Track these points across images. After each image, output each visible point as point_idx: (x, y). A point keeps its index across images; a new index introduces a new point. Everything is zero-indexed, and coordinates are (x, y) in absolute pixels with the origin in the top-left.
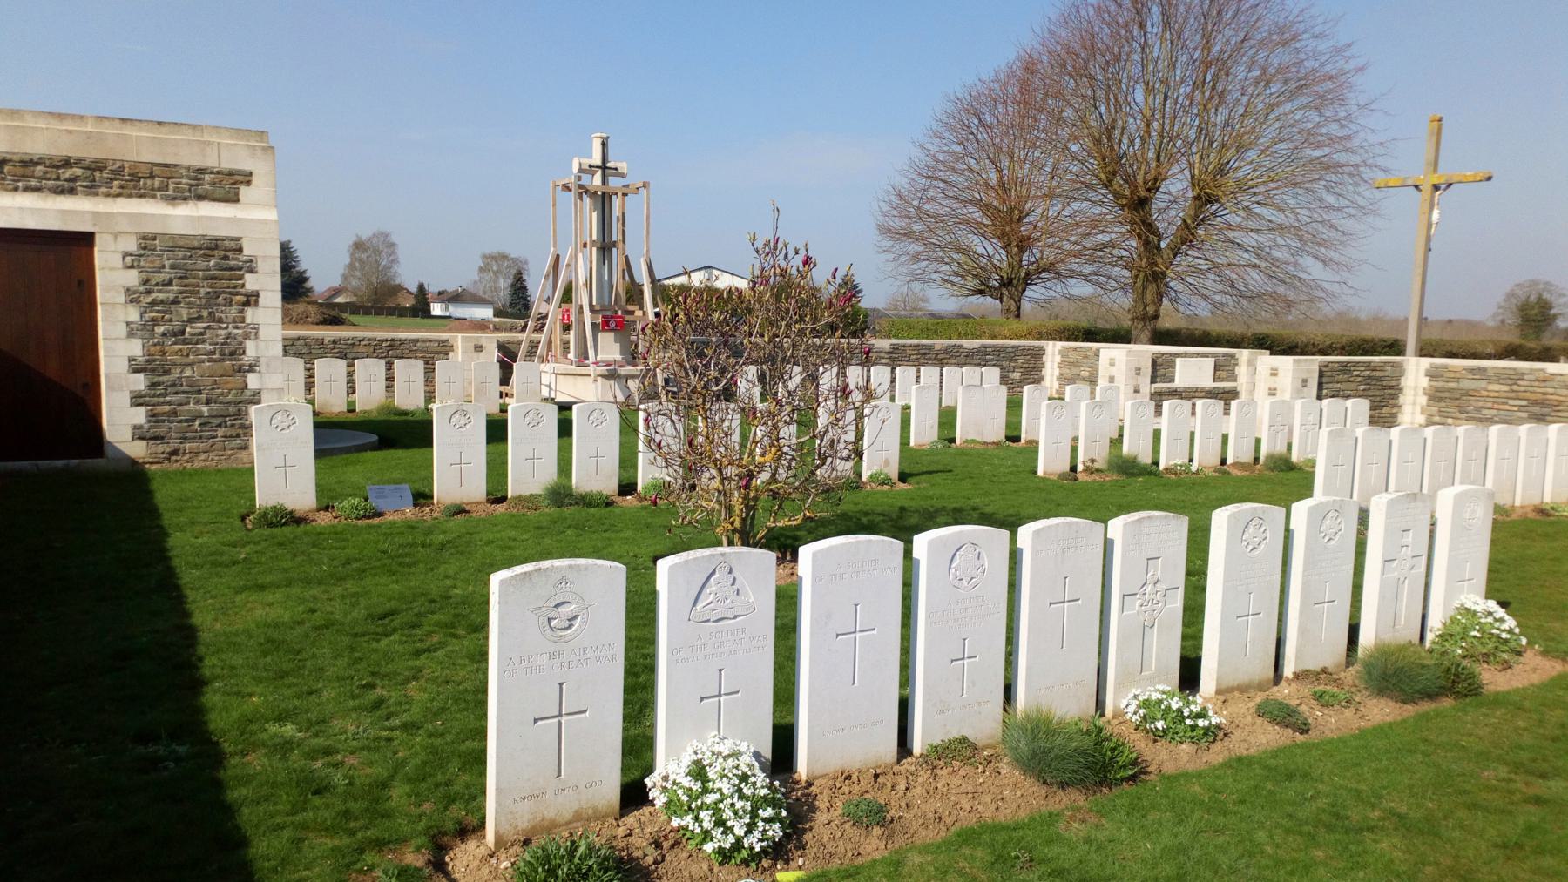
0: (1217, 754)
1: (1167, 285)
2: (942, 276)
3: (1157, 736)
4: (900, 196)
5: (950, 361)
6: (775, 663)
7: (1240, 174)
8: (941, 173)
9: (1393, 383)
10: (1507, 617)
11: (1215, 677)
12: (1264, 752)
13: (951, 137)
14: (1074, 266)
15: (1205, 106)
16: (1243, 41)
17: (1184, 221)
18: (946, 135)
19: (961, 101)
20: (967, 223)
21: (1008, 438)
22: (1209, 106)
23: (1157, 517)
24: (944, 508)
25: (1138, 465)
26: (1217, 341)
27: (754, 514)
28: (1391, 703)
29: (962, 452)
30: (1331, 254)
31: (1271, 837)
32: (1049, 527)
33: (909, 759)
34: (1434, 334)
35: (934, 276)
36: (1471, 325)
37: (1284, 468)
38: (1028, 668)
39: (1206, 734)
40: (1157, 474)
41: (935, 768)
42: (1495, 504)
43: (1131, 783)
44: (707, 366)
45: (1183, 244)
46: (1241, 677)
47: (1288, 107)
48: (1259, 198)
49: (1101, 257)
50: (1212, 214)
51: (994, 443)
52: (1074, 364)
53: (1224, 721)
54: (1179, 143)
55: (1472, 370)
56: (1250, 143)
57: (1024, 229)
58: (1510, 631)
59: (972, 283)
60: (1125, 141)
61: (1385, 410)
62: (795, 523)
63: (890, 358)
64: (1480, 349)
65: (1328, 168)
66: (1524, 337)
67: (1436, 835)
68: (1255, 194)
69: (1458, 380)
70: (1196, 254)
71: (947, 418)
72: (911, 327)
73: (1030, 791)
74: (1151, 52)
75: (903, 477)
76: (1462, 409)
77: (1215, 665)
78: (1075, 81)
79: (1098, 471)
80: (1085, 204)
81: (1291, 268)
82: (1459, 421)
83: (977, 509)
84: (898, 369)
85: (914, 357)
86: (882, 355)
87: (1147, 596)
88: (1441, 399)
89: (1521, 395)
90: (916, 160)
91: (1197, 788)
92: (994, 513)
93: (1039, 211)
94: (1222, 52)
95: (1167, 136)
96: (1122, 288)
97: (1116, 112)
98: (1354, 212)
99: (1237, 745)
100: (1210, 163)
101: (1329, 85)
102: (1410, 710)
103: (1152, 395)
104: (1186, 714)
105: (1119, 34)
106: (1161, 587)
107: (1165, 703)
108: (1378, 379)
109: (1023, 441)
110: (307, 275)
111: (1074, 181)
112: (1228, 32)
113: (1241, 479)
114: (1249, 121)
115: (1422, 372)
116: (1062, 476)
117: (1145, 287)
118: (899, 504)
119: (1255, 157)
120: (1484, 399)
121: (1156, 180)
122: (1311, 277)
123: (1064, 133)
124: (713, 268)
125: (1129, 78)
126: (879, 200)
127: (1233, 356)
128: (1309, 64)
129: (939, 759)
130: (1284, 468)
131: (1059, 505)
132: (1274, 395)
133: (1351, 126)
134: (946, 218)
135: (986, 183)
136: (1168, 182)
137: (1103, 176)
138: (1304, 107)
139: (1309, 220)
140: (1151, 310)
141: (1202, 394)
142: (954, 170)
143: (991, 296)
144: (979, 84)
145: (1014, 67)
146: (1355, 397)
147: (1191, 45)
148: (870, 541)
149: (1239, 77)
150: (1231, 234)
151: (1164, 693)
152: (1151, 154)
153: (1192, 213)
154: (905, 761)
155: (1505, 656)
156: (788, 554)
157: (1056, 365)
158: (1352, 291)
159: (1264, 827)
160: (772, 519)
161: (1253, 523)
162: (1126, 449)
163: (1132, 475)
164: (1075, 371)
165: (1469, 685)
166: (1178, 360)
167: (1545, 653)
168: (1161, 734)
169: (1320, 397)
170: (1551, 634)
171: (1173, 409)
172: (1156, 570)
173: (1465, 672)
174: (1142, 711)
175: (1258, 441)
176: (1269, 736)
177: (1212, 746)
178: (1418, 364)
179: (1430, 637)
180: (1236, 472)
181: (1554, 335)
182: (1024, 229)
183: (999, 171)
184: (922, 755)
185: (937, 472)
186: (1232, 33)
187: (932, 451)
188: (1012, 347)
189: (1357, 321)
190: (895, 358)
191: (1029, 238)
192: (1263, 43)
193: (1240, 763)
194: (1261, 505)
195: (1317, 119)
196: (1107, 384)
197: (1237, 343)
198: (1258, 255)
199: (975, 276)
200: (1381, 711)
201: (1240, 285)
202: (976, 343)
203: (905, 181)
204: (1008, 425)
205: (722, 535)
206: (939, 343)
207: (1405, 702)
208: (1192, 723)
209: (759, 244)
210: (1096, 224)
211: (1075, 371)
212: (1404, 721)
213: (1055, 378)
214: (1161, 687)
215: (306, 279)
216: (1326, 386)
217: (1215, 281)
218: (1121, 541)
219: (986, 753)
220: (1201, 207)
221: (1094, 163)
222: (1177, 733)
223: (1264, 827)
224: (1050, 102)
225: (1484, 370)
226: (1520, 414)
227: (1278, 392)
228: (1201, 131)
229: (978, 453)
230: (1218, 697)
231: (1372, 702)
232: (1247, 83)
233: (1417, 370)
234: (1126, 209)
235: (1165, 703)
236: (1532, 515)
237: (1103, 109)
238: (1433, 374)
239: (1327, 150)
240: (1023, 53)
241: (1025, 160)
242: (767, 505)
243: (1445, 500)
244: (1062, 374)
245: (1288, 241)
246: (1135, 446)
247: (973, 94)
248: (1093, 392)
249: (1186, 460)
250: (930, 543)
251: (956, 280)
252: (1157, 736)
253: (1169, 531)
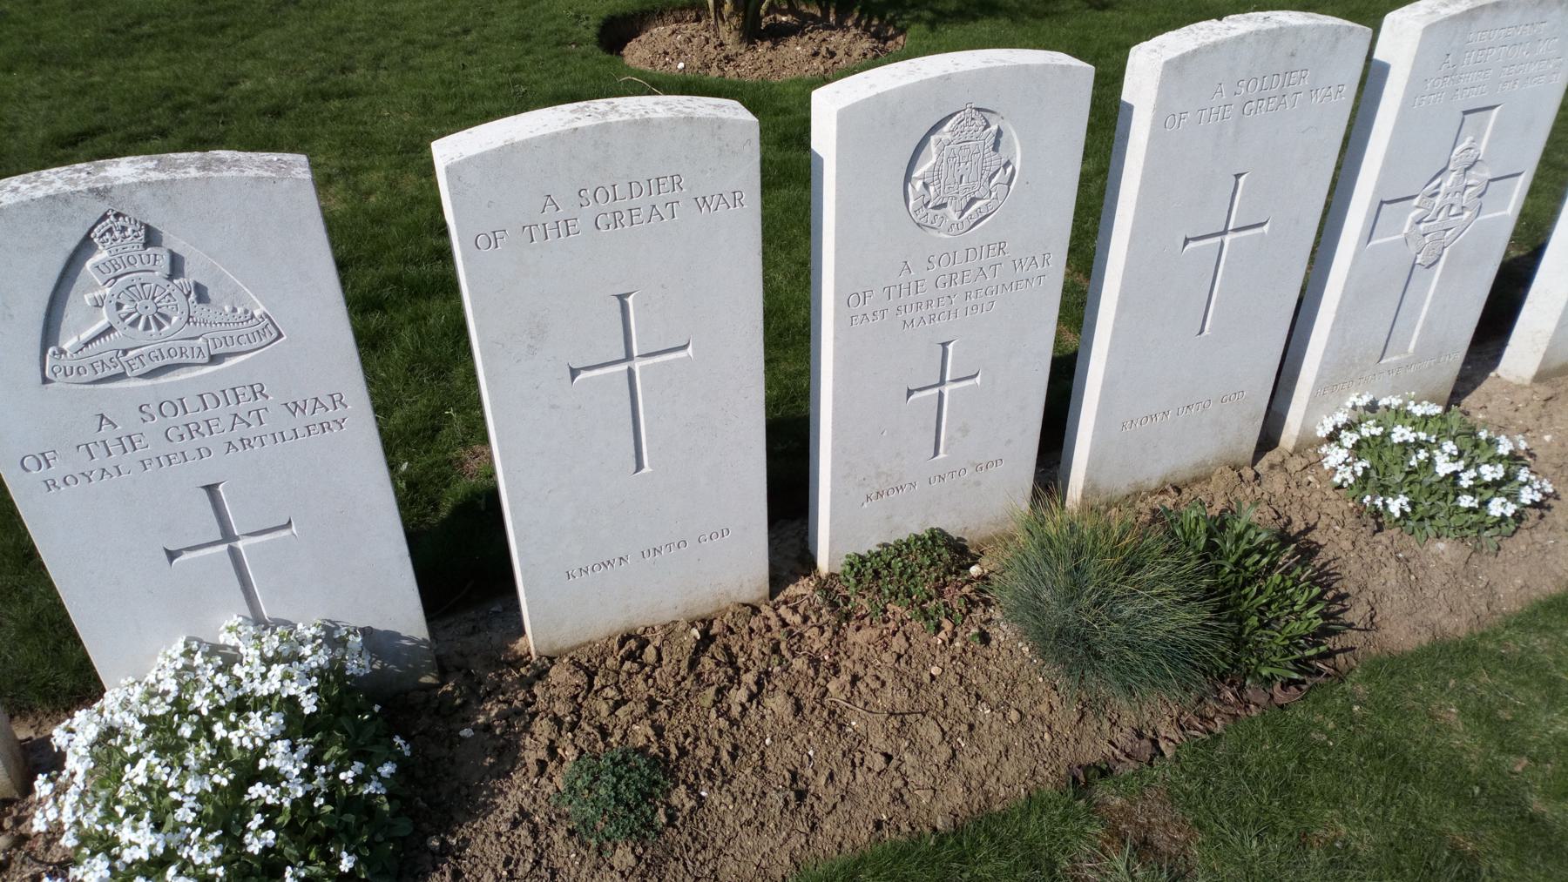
6: (765, 219)
11: (1543, 348)
87: (1438, 200)
148: (646, 123)
156: (832, 11)
177: (1507, 543)
218: (1407, 71)
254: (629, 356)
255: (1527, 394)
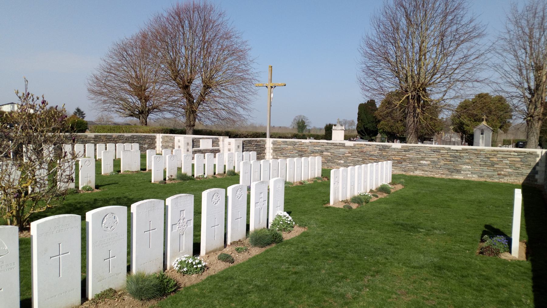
0: (205, 276)
1: (196, 115)
2: (116, 109)
3: (184, 273)
4: (97, 78)
5: (120, 141)
7: (217, 79)
8: (113, 71)
9: (263, 146)
10: (289, 217)
12: (219, 272)
13: (116, 58)
14: (165, 107)
15: (205, 56)
16: (215, 36)
17: (201, 94)
18: (114, 57)
19: (119, 45)
20: (124, 90)
21: (141, 169)
22: (206, 56)
23: (183, 196)
24: (113, 198)
25: (187, 176)
26: (214, 134)
27: (23, 208)
28: (258, 248)
29: (123, 176)
30: (245, 106)
31: (219, 303)
32: (143, 203)
33: (87, 302)
34: (275, 131)
35: (113, 109)
36: (285, 128)
37: (233, 174)
38: (137, 257)
39: (201, 270)
40: (193, 179)
41: (98, 303)
42: (286, 183)
43: (174, 293)
45: (201, 101)
46: (214, 247)
47: (230, 59)
48: (223, 87)
49: (174, 104)
50: (210, 92)
51: (136, 171)
52: (167, 142)
53: (207, 264)
54: (197, 68)
55: (283, 142)
56: (219, 70)
57: (147, 94)
58: (290, 221)
59: (128, 112)
60: (180, 65)
61: (262, 154)
62: (43, 210)
63: (94, 140)
64: (287, 135)
65: (243, 79)
66: (299, 131)
67: (268, 290)
68: (222, 86)
69: (280, 145)
70: (205, 105)
71: (117, 163)
72: (104, 128)
73: (136, 304)
74: (186, 36)
75: (97, 187)
76: (282, 154)
77: (205, 244)
78: (161, 43)
79: (173, 179)
80: (168, 86)
81: (234, 110)
82: (281, 157)
83: (126, 197)
84: (97, 145)
85: (105, 140)
86: (91, 139)
88: (276, 151)
89: (296, 149)
90: (103, 66)
91: (196, 290)
92: (133, 198)
93: (152, 87)
94: (209, 39)
95: (193, 65)
96: (182, 115)
97: (176, 55)
98: (251, 93)
99: (211, 272)
100: (208, 75)
101: (241, 53)
102: (264, 249)
103: (193, 152)
104: (194, 264)
105: (175, 28)
106: (186, 220)
107: (187, 261)
108: (259, 145)
109: (147, 170)
111: (163, 78)
112: (210, 33)
113: (219, 179)
114: (219, 63)
115: (271, 143)
116: (161, 182)
117: (190, 116)
118: (94, 198)
119: (221, 74)
120: (287, 150)
121: (191, 79)
122: (240, 113)
123: (159, 61)
124: (15, 104)
125: (180, 44)
126: (88, 79)
127: (218, 139)
128: (235, 46)
129: (100, 299)
130: (233, 174)
131: (158, 193)
132: (230, 151)
133: (248, 67)
134: (116, 88)
135: (132, 77)
136: (195, 80)
137: (173, 77)
138: (234, 59)
139: (238, 95)
140: (192, 123)
141: (209, 151)
142: (118, 70)
143: (136, 117)
144: (125, 40)
145: (139, 36)
146: (253, 151)
147: (199, 35)
148: (65, 217)
149: (215, 48)
150: (215, 99)
151: (187, 258)
152: (189, 71)
153: (203, 91)
154: (85, 303)
155: (289, 228)
157: (160, 142)
158: (251, 118)
159: (217, 299)
160: (32, 209)
161: (215, 195)
162: (183, 171)
163: (185, 180)
164: (167, 144)
165: (279, 239)
166: (201, 140)
167: (300, 226)
168: (186, 272)
169: (243, 151)
170: (301, 220)
171: (208, 156)
172: (183, 215)
173: (278, 235)
174: (179, 266)
175: (225, 166)
176: (222, 266)
177: (203, 273)
178: (269, 141)
179: (270, 225)
180: (218, 177)
181: (306, 131)
182: (147, 94)
183: (136, 72)
184: (92, 299)
185: (112, 184)
186: (211, 33)
187: (111, 176)
188: (144, 136)
189: (255, 127)
190: (96, 140)
191: (149, 97)
192: (221, 37)
193: (212, 277)
194: (218, 189)
195: (239, 64)
196: (178, 148)
197: (220, 134)
198: (224, 106)
199: (129, 110)
200: (256, 251)
201: (219, 115)
202: (130, 135)
203: (98, 73)
204: (141, 165)
205: (7, 219)
206: (115, 135)
207: (262, 247)
208: (196, 266)
209: (20, 94)
210: (171, 92)
211: (167, 144)
212: (261, 254)
213: (160, 147)
214: (186, 256)
216: (245, 148)
217: (212, 114)
219: (119, 293)
220: (206, 89)
221: (170, 72)
222: (191, 271)
223: (217, 299)
224: (153, 49)
225: (286, 142)
226: (296, 155)
227: (231, 150)
228: (204, 64)
229: (130, 176)
230: (207, 255)
231: (253, 249)
232: (217, 50)
233: (269, 142)
234: (512, 107)
235: (187, 261)
236: (299, 184)
237: (171, 54)
238: (274, 143)
239: (242, 74)
240: (142, 31)
241: (145, 69)
242: (30, 203)
243: (272, 183)
244: (162, 145)
245: (233, 102)
246: (186, 170)
247: (124, 43)
248: (172, 151)
249: (203, 174)
250: (93, 215)
251: (122, 111)
252: (184, 273)
253: (187, 200)
254: (59, 255)
255: (205, 257)
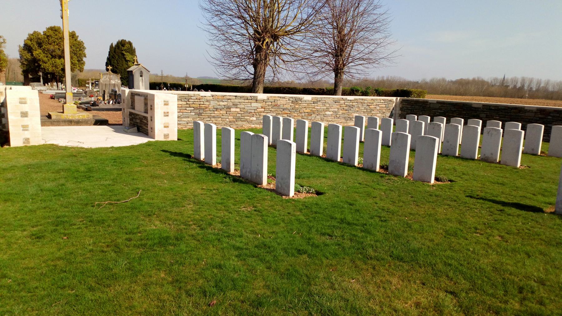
44: (358, 107)
110: (540, 79)
215: (538, 79)
